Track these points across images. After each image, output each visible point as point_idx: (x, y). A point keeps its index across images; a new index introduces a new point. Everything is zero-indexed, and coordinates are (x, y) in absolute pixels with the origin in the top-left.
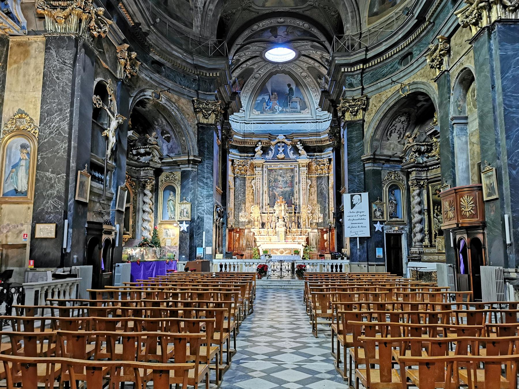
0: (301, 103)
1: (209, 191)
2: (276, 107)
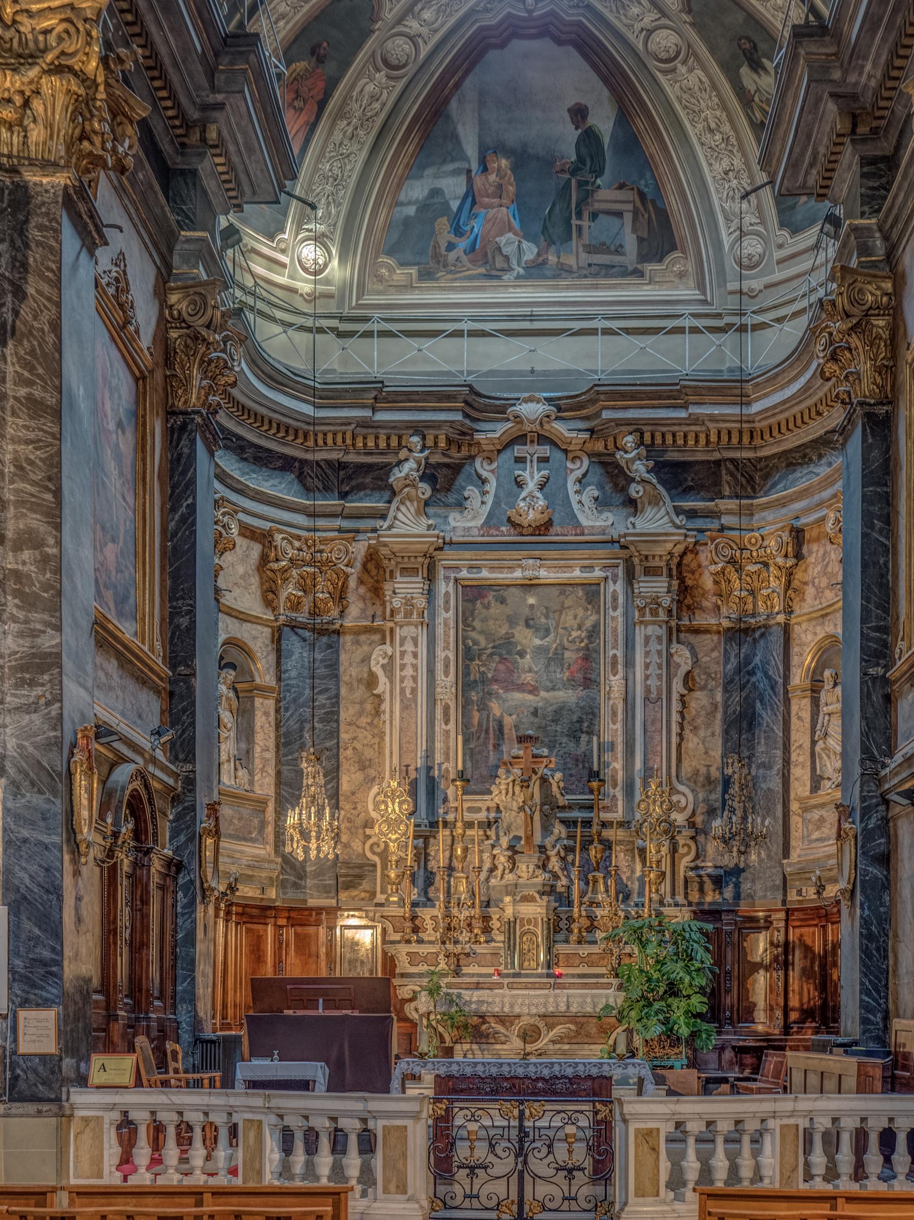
0: (643, 220)
1: (34, 634)
2: (508, 241)
